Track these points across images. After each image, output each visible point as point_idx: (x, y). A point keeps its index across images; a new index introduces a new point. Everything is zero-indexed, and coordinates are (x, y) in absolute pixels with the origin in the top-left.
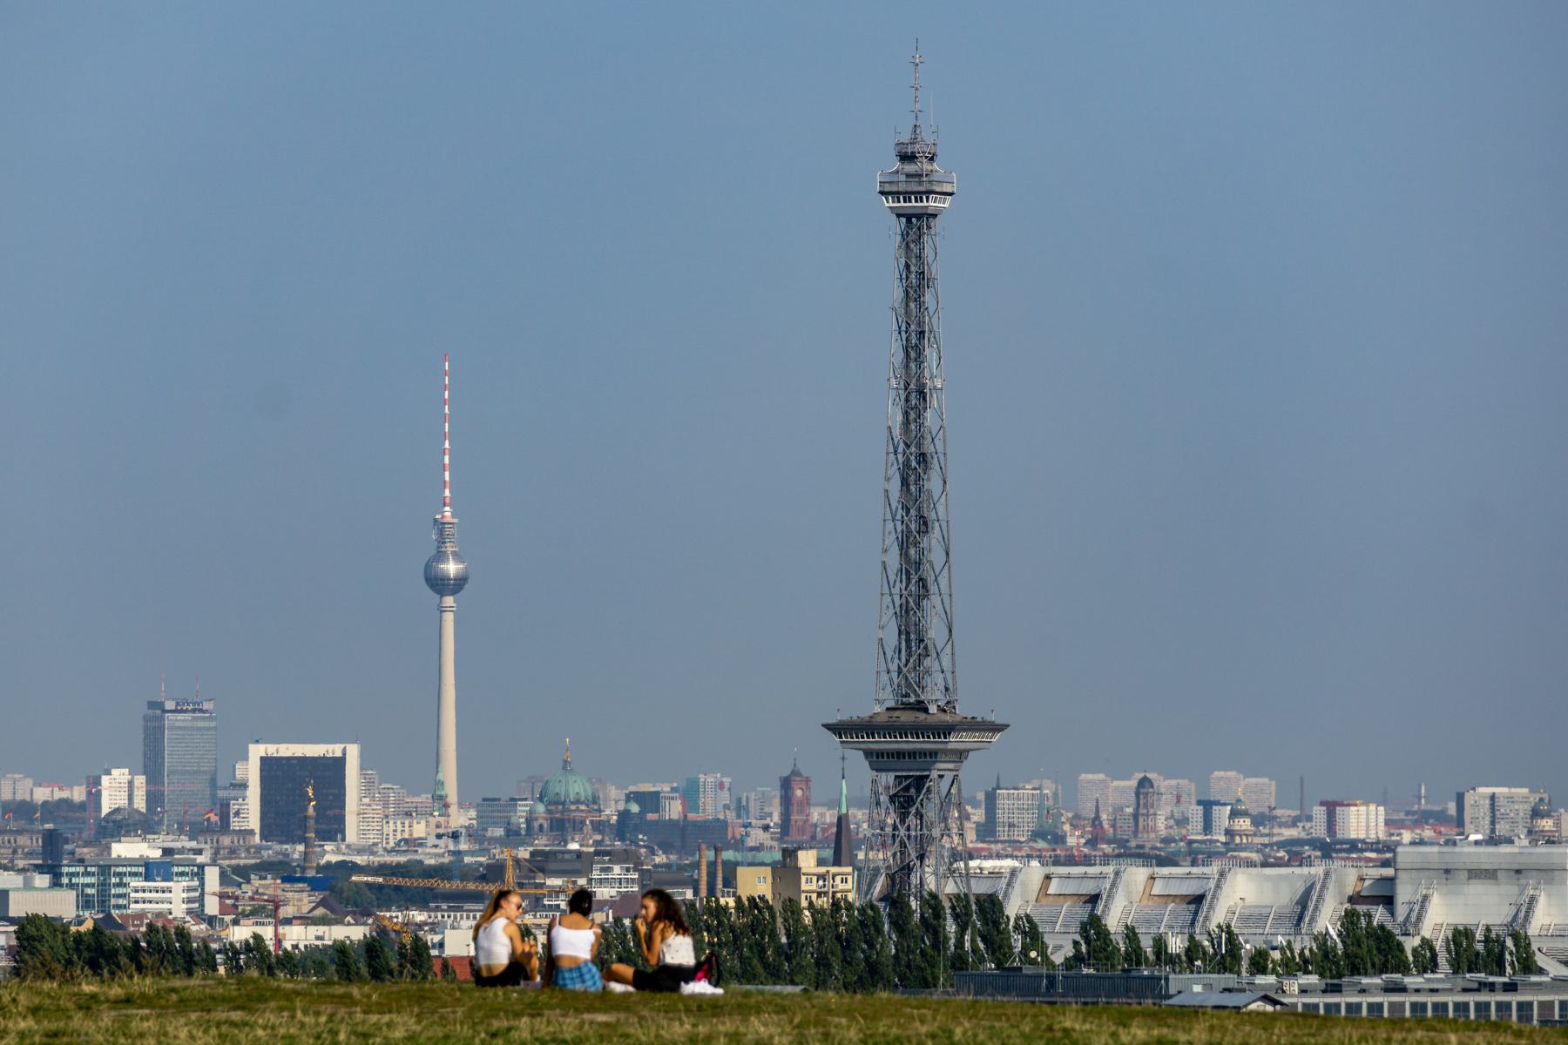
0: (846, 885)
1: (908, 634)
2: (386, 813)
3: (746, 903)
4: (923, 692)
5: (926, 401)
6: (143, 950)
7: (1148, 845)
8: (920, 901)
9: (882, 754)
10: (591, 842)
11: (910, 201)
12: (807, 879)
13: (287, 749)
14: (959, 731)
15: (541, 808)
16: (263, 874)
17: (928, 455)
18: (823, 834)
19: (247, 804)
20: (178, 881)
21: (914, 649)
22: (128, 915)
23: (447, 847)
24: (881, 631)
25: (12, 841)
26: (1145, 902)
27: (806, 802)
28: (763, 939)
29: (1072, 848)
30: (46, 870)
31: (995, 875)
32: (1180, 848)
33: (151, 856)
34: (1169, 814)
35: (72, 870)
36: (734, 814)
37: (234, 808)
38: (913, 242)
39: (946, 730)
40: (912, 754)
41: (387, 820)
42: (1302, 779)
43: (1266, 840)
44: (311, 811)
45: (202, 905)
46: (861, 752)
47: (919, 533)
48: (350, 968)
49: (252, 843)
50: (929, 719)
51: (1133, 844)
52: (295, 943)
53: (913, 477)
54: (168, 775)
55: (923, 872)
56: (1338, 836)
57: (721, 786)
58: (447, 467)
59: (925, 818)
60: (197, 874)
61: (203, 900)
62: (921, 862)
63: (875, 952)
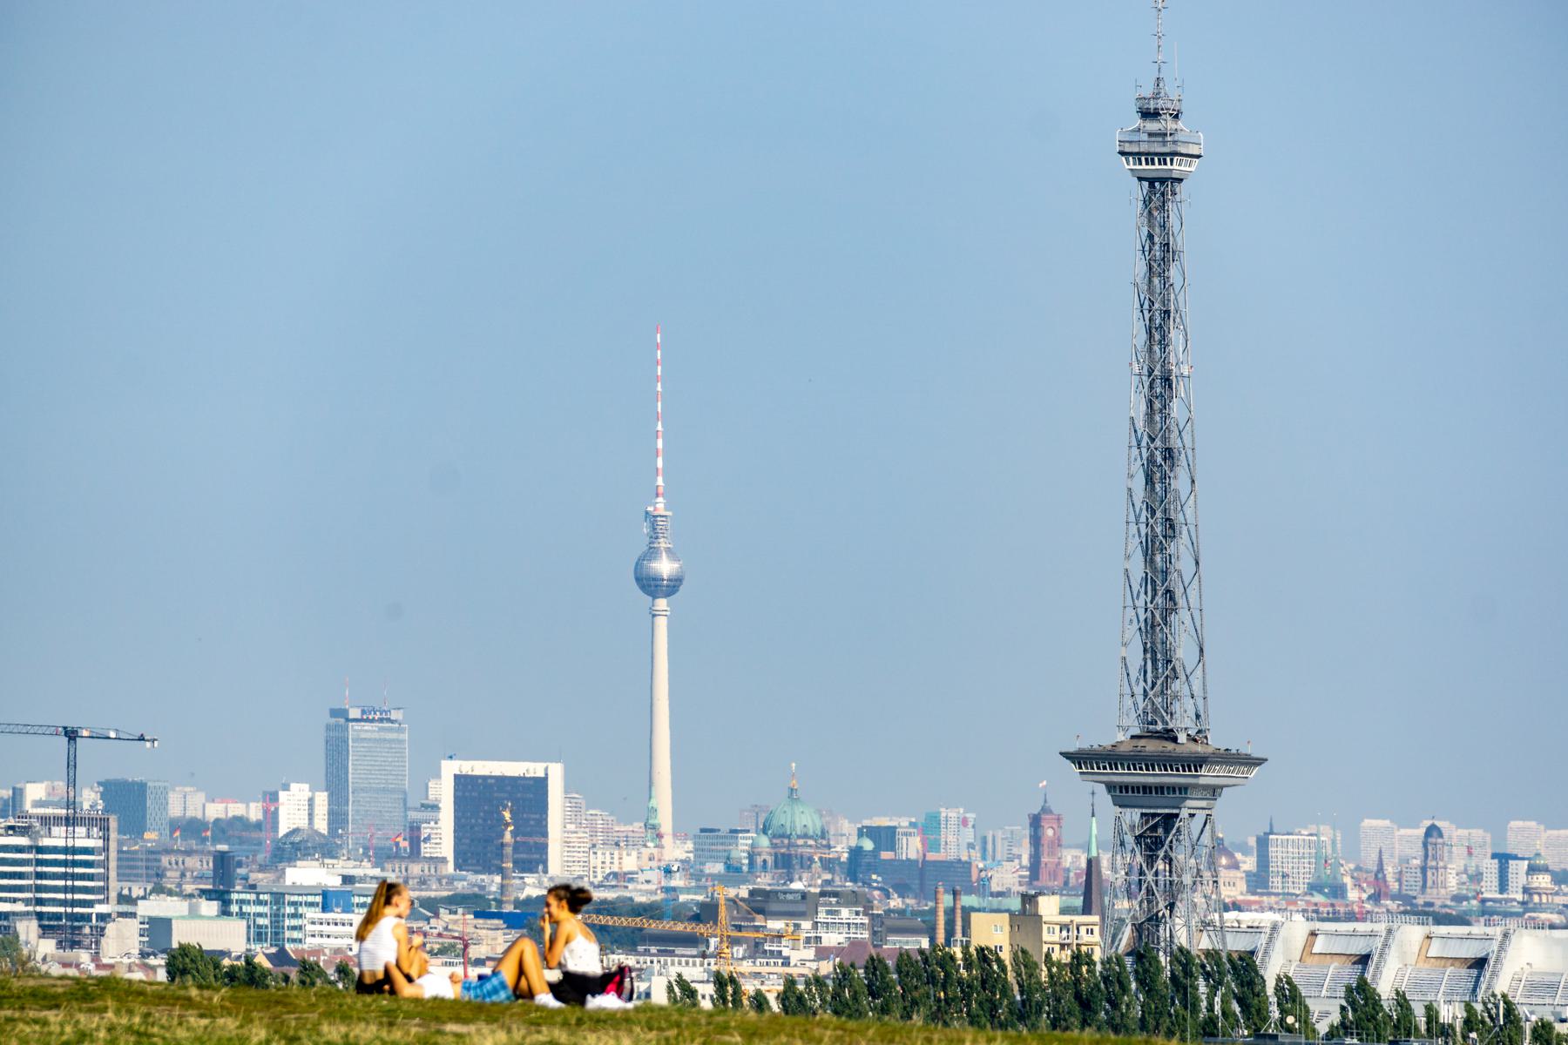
0: (1094, 942)
1: (1154, 653)
2: (594, 842)
3: (975, 953)
5: (1172, 390)
7: (1438, 903)
8: (1171, 956)
9: (1127, 788)
10: (819, 882)
11: (1153, 164)
12: (1049, 928)
14: (1213, 763)
15: (764, 841)
16: (453, 908)
18: (1077, 880)
21: (1160, 671)
23: (660, 883)
24: (1124, 648)
25: (180, 862)
26: (1420, 965)
27: (1058, 843)
28: (995, 995)
29: (1353, 903)
30: (213, 896)
31: (1254, 929)
33: (329, 885)
34: (1462, 868)
35: (243, 896)
36: (979, 855)
37: (424, 833)
38: (1157, 209)
39: (1198, 762)
40: (1160, 789)
44: (508, 837)
46: (1103, 786)
47: (1165, 537)
49: (444, 873)
50: (1179, 749)
51: (1420, 901)
53: (1158, 475)
54: (353, 793)
57: (965, 822)
58: (660, 472)
59: (1175, 862)
62: (1171, 912)
63: (1119, 1014)
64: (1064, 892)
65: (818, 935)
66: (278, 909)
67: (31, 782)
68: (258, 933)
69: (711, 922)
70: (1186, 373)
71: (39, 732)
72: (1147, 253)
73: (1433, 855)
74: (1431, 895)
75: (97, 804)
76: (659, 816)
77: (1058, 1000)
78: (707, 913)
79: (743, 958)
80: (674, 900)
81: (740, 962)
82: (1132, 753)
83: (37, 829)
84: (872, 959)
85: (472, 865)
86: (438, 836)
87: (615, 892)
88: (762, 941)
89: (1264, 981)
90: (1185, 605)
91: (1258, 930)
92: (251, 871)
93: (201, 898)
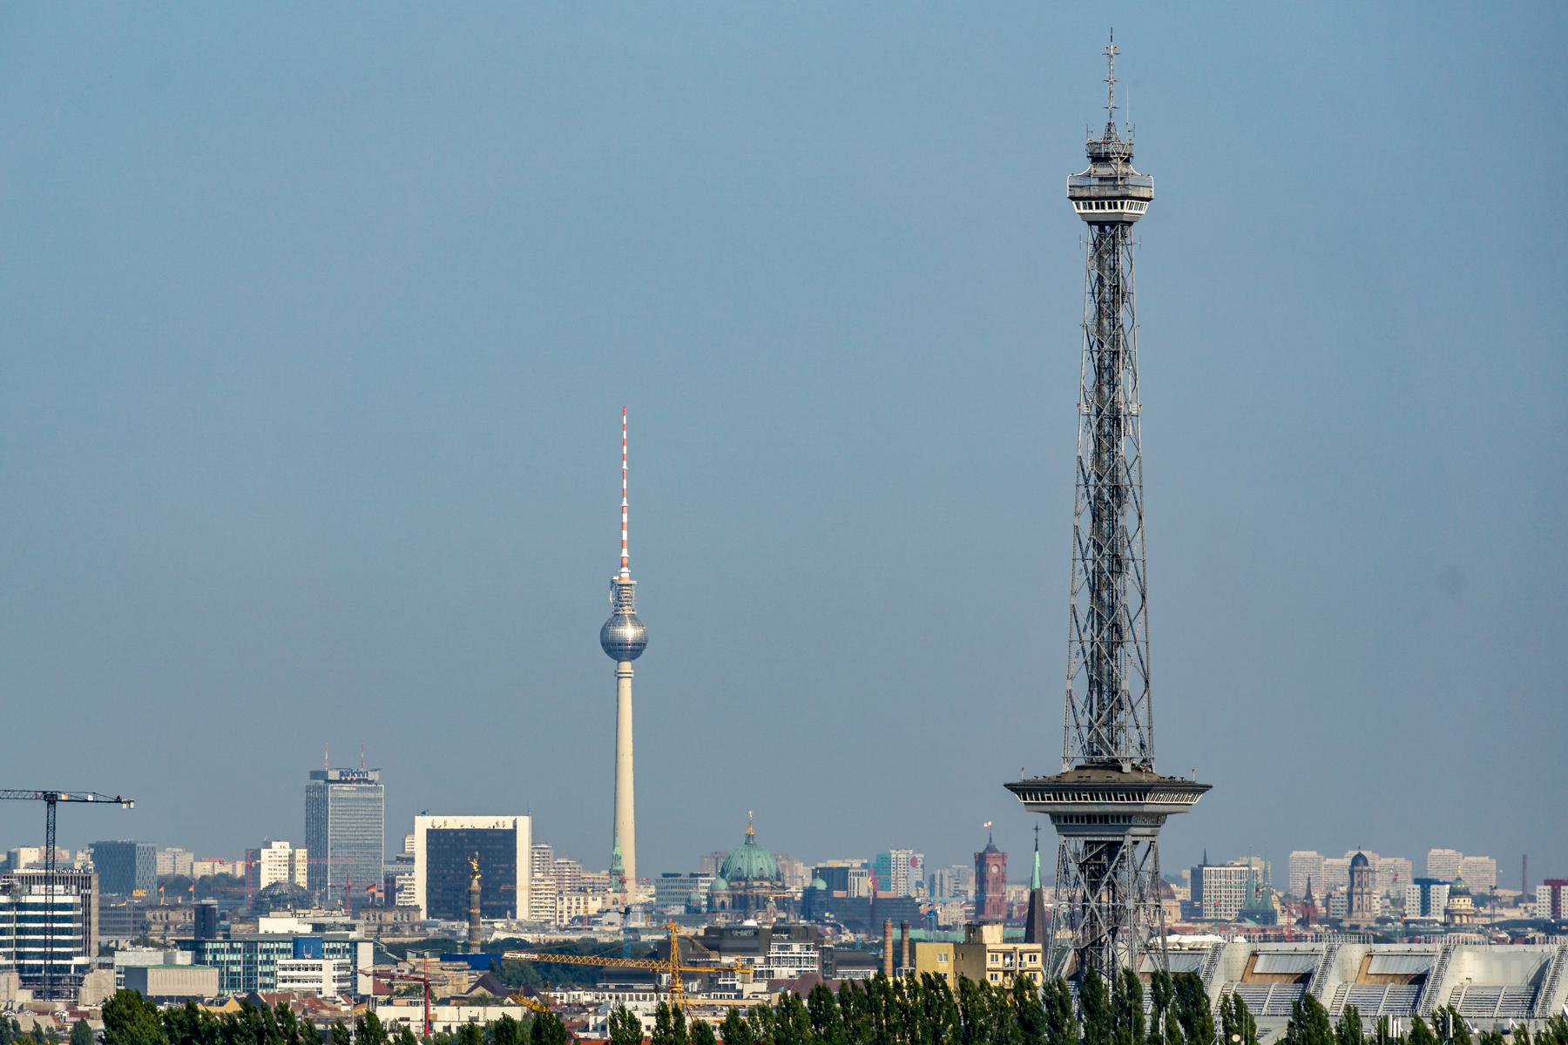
0: (1034, 965)
1: (1100, 684)
4: (1116, 749)
7: (1364, 925)
9: (1071, 818)
11: (1103, 208)
12: (992, 956)
14: (1156, 792)
16: (420, 952)
18: (1020, 913)
20: (329, 959)
24: (1069, 682)
25: (164, 917)
27: (1002, 879)
28: (938, 1020)
29: (1282, 927)
31: (1196, 951)
32: (1397, 928)
33: (300, 932)
34: (1385, 894)
39: (1143, 790)
40: (1104, 818)
42: (1524, 857)
43: (1487, 921)
44: (475, 884)
45: (355, 985)
47: (1111, 572)
49: (416, 920)
50: (1123, 779)
51: (1346, 924)
52: (447, 1024)
53: (1106, 512)
54: (331, 849)
56: (1562, 916)
57: (914, 862)
58: (625, 526)
60: (348, 951)
62: (1114, 936)
64: (1008, 924)
65: (771, 969)
66: (251, 957)
67: (24, 847)
68: (231, 980)
69: (663, 959)
71: (4, 796)
72: (1096, 296)
73: (1359, 882)
74: (1357, 917)
75: (88, 864)
78: (661, 951)
79: (698, 992)
80: (636, 940)
83: (18, 887)
84: (818, 989)
85: (443, 912)
86: (412, 887)
87: (580, 934)
88: (716, 976)
89: (1209, 1001)
91: (1200, 952)
92: (232, 923)
93: (176, 948)
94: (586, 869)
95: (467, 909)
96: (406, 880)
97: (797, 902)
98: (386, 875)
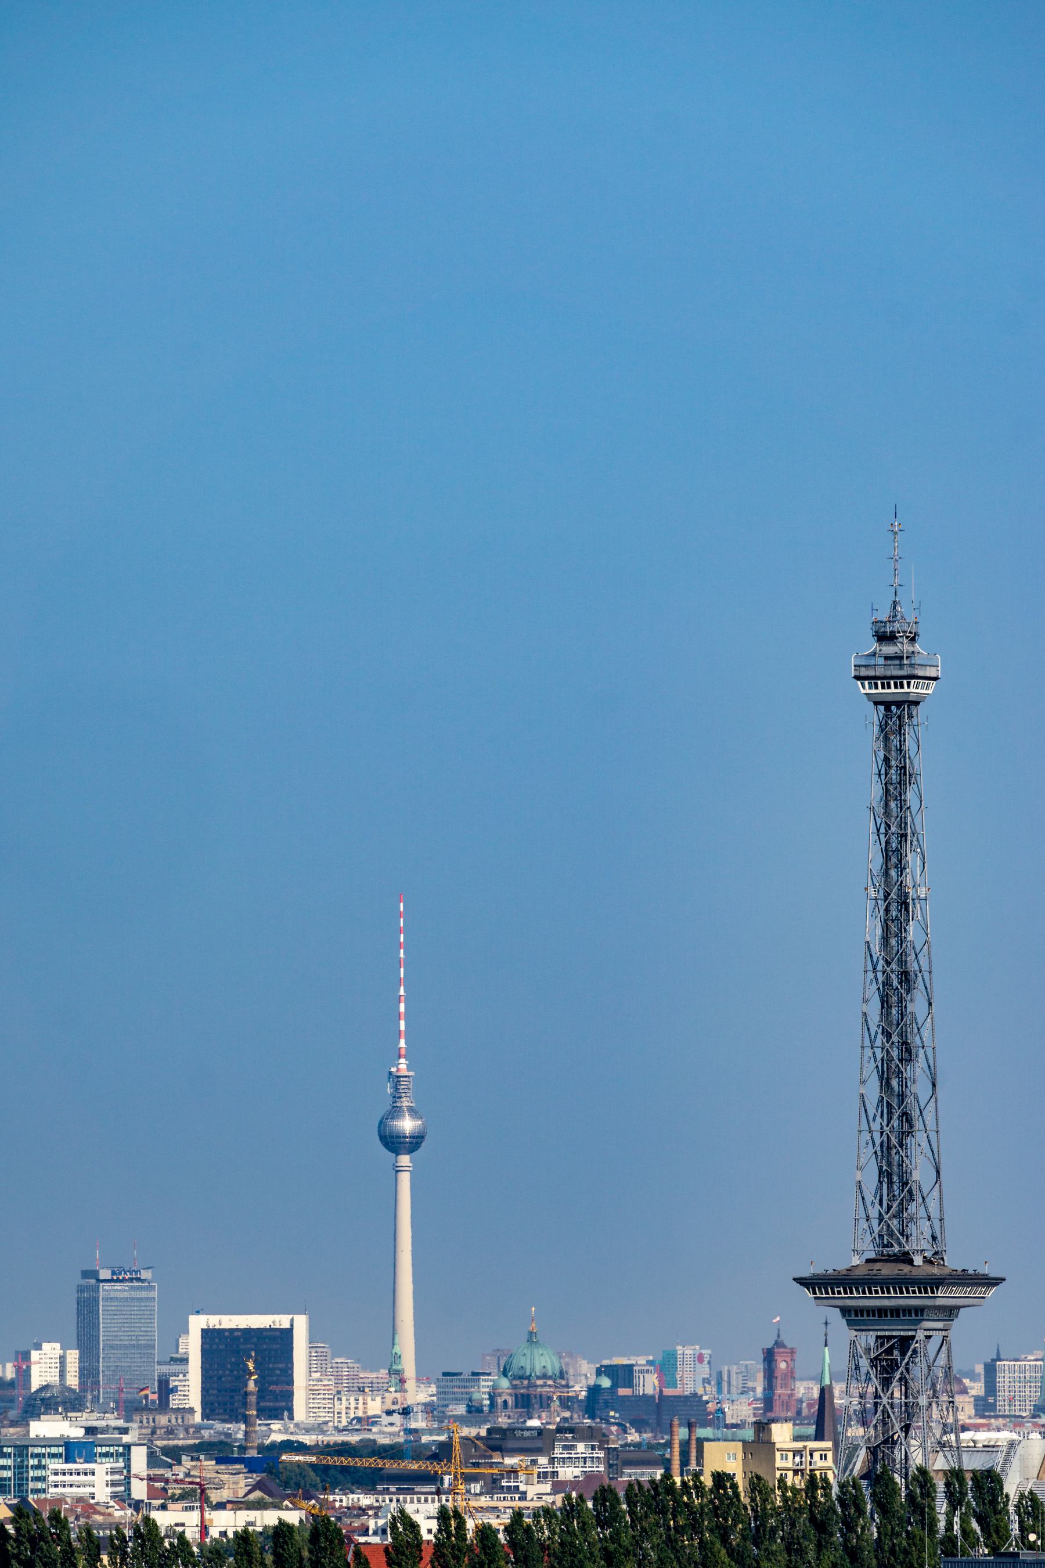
1: (890, 1175)
2: (339, 1389)
4: (907, 1241)
5: (908, 912)
6: (11, 1537)
10: (558, 1419)
11: (889, 687)
12: (782, 1455)
13: (230, 1320)
17: (912, 974)
18: (809, 1410)
19: (188, 1380)
20: (101, 1463)
22: (45, 1499)
24: (859, 1172)
27: (791, 1375)
31: (990, 1448)
33: (72, 1436)
39: (936, 1283)
40: (896, 1312)
41: (339, 1396)
44: (251, 1386)
47: (901, 1060)
48: (252, 1557)
49: (191, 1422)
50: (915, 1272)
52: (223, 1529)
53: (895, 999)
55: (909, 1446)
58: (402, 1016)
60: (122, 1455)
61: (129, 1483)
64: (797, 1422)
65: (555, 1470)
66: (22, 1461)
70: (923, 896)
76: (403, 1362)
77: (793, 1525)
78: (443, 1452)
79: (481, 1494)
81: (478, 1497)
82: (867, 1277)
85: (219, 1414)
88: (499, 1477)
90: (922, 1127)
91: (994, 1449)
94: (365, 1369)
95: (242, 1410)
96: (180, 1381)
97: (581, 1401)
98: (159, 1376)
